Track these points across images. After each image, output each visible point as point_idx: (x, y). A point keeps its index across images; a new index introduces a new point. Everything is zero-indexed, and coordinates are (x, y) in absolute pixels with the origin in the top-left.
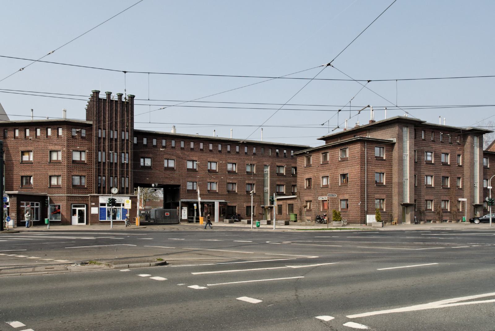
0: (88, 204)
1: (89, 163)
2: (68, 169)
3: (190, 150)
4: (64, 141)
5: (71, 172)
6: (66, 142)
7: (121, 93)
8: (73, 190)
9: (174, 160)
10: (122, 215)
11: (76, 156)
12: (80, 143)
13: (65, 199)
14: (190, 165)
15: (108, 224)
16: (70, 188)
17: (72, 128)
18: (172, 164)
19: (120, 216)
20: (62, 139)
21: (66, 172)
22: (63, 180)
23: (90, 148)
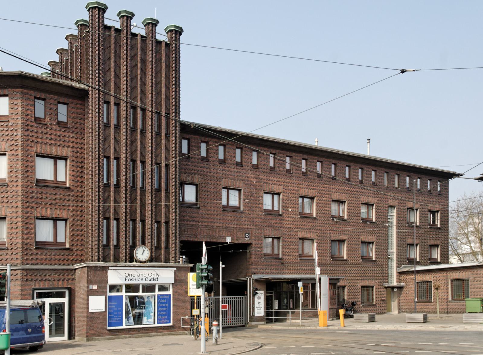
0: (72, 287)
1: (77, 187)
2: (26, 200)
3: (268, 170)
4: (16, 130)
5: (32, 208)
6: (20, 133)
7: (155, 18)
8: (36, 254)
9: (240, 190)
10: (158, 311)
11: (44, 170)
12: (54, 138)
13: (19, 277)
14: (267, 202)
15: (128, 336)
16: (31, 250)
17: (36, 98)
18: (234, 199)
19: (152, 314)
20: (10, 123)
21: (20, 210)
22: (13, 230)
23: (78, 152)
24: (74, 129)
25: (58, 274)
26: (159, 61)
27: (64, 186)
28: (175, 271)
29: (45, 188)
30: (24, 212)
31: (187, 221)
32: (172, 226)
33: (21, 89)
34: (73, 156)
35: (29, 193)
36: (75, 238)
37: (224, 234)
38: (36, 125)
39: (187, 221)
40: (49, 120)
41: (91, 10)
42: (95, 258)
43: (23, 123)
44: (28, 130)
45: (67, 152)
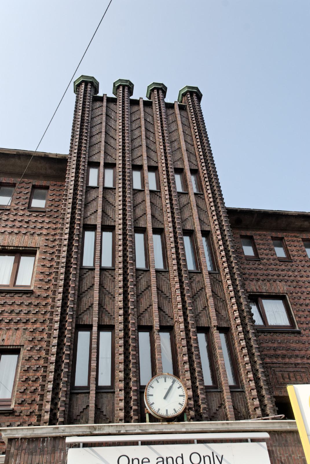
31: (284, 357)
39: (284, 357)
45: (37, 241)
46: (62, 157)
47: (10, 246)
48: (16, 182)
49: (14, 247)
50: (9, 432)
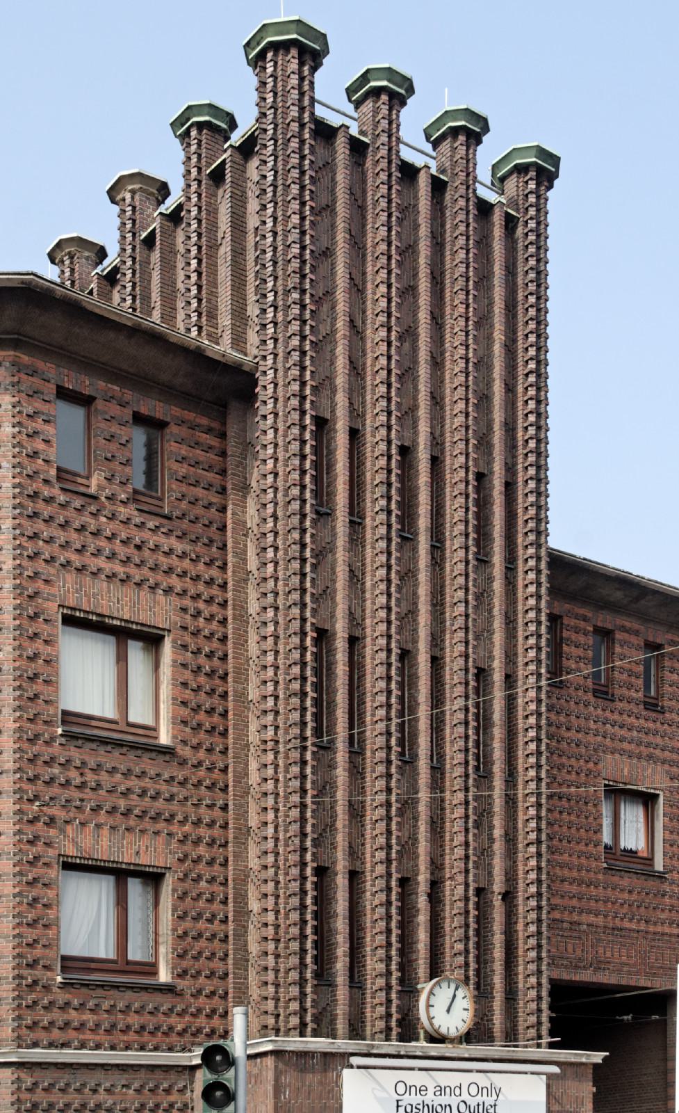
1: (196, 748)
2: (31, 790)
5: (51, 822)
24: (185, 524)
25: (136, 1085)
26: (484, 280)
27: (151, 741)
28: (550, 1076)
29: (94, 746)
30: (25, 838)
32: (525, 907)
33: (12, 353)
34: (184, 628)
35: (40, 762)
36: (192, 948)
37: (609, 954)
38: (62, 498)
40: (104, 482)
41: (270, 55)
42: (287, 1022)
43: (19, 485)
44: (36, 514)
45: (155, 610)
46: (234, 363)
47: (113, 618)
48: (93, 394)
49: (121, 620)
50: (280, 1043)
